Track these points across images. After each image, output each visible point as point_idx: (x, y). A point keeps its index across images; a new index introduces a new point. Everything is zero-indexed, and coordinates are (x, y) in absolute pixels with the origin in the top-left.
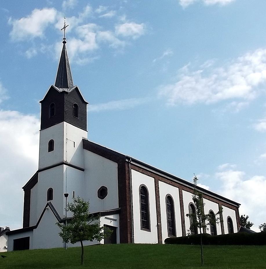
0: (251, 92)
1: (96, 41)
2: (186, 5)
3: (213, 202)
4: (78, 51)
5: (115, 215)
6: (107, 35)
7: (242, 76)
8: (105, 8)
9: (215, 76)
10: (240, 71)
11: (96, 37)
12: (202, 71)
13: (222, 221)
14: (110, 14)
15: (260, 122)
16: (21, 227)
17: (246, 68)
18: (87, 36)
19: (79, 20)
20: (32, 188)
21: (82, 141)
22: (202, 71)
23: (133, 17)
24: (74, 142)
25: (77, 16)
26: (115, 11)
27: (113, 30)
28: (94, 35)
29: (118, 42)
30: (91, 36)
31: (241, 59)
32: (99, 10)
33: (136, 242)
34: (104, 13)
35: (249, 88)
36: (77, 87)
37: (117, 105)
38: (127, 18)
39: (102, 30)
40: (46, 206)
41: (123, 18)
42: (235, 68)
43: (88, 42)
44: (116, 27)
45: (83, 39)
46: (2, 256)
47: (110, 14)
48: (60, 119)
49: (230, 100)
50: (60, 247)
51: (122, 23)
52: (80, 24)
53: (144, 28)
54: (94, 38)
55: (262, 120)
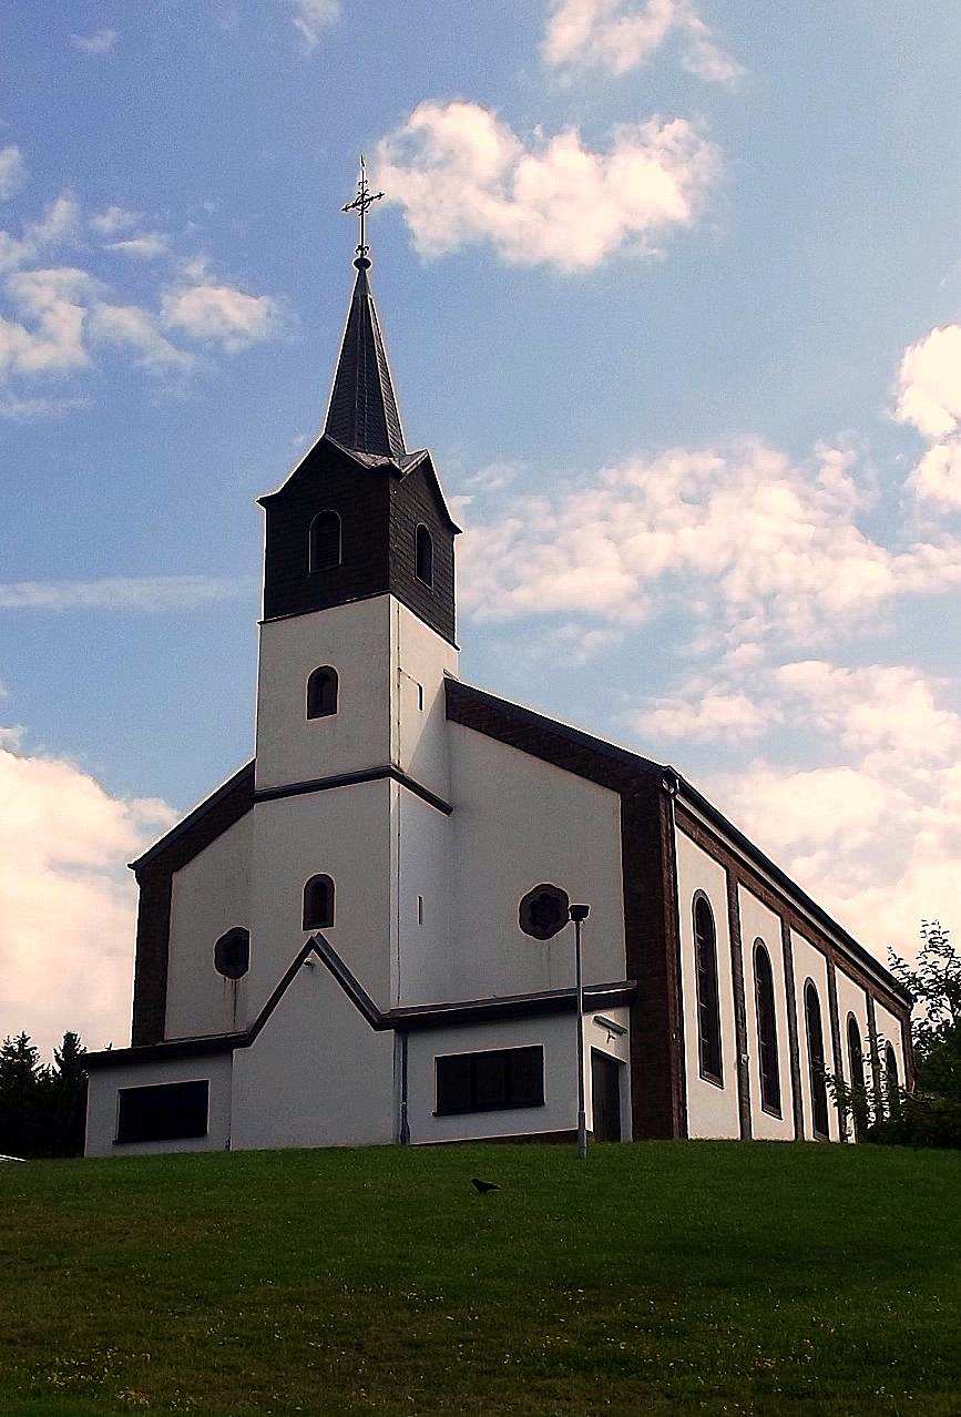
0: (633, 597)
1: (85, 341)
2: (437, 252)
3: (855, 981)
4: (10, 367)
5: (619, 1011)
6: (127, 321)
7: (608, 537)
8: (129, 219)
9: (514, 525)
10: (605, 517)
11: (85, 322)
12: (468, 500)
13: (742, 1067)
14: (146, 246)
15: (656, 709)
16: (122, 1039)
17: (625, 509)
18: (47, 317)
19: (21, 251)
20: (177, 870)
21: (441, 688)
22: (468, 500)
23: (234, 269)
24: (421, 688)
25: (18, 235)
26: (165, 237)
27: (154, 307)
28: (80, 312)
29: (168, 353)
30: (66, 320)
31: (610, 476)
32: (106, 223)
33: (696, 1130)
34: (121, 236)
35: (628, 582)
36: (428, 457)
37: (132, 593)
38: (209, 270)
39: (110, 301)
40: (304, 954)
41: (196, 269)
42: (586, 505)
43: (51, 338)
44: (166, 300)
45: (32, 326)
46: (475, 1182)
47: (146, 246)
48: (367, 580)
49: (557, 618)
50: (373, 1140)
51: (191, 284)
52: (26, 266)
53: (269, 314)
54: (77, 325)
55: (664, 700)
